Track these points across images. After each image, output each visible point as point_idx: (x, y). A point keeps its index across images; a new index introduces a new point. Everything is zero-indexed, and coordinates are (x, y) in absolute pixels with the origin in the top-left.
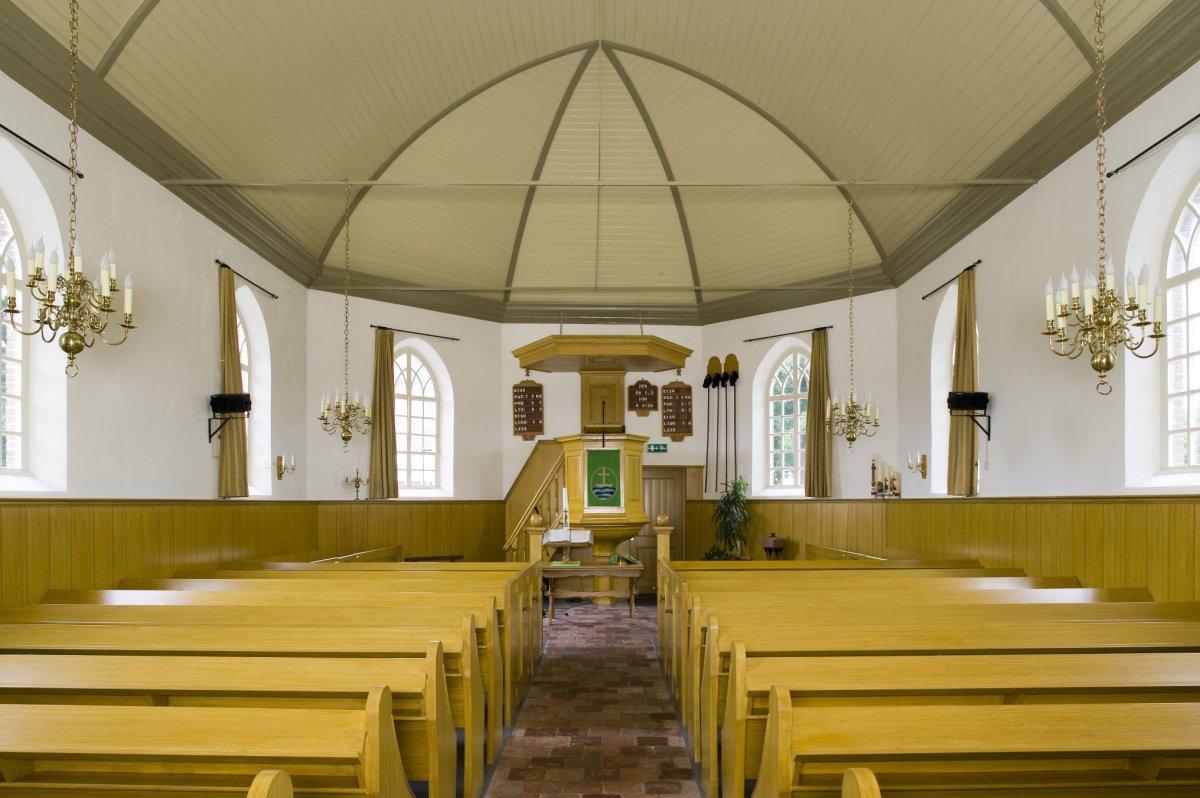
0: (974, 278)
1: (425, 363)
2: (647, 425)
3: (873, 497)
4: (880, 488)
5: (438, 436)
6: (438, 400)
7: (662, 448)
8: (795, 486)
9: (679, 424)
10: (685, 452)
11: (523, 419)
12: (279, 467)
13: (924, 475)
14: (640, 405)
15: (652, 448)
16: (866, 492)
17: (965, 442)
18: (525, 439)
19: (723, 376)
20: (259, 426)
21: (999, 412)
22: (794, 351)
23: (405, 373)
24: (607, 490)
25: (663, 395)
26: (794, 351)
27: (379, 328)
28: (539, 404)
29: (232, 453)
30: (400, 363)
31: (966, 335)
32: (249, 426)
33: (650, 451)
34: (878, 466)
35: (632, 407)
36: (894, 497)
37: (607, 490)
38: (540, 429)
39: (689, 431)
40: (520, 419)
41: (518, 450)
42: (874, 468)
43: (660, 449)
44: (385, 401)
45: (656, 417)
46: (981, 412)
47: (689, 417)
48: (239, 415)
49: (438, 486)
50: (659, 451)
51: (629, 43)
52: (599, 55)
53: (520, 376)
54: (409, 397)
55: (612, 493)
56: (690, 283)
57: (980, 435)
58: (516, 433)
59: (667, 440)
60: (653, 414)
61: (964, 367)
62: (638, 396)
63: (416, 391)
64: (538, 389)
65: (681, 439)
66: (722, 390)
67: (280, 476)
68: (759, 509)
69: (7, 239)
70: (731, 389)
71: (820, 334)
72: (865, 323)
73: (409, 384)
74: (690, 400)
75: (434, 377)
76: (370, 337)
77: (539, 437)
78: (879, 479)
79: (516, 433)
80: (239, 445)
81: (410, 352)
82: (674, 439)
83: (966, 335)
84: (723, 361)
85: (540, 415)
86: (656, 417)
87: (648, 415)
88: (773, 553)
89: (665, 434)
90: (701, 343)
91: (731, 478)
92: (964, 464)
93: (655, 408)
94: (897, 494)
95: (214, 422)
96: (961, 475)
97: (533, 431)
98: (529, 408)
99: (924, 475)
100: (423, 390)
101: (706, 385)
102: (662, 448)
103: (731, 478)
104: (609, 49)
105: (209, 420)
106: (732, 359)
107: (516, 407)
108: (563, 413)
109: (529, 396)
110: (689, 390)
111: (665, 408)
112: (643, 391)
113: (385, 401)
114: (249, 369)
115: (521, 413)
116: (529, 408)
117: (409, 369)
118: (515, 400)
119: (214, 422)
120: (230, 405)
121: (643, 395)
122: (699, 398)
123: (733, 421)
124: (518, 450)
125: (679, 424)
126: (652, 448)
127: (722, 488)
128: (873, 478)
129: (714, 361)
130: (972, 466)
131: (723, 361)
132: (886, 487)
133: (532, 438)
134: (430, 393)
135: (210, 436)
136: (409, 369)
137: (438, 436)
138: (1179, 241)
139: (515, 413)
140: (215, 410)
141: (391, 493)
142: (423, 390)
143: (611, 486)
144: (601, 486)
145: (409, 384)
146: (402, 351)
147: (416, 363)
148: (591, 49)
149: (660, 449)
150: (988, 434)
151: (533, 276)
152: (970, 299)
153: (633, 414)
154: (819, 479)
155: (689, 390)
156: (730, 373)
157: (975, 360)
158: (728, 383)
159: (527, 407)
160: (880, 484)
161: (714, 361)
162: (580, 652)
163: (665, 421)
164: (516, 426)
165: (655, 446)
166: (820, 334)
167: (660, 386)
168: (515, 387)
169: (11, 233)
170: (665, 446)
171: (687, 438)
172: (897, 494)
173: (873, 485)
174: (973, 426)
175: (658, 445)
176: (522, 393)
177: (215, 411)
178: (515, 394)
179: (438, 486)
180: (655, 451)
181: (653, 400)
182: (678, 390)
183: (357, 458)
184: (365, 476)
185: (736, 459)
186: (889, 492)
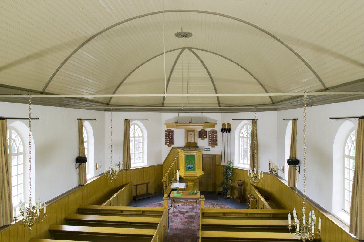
0: (296, 123)
1: (139, 127)
2: (203, 143)
3: (269, 172)
4: (272, 170)
5: (143, 147)
6: (143, 137)
7: (208, 149)
8: (247, 164)
9: (214, 142)
10: (216, 151)
11: (168, 141)
12: (97, 167)
13: (283, 172)
14: (202, 136)
15: (206, 149)
16: (267, 171)
17: (293, 172)
18: (169, 146)
19: (226, 129)
20: (90, 166)
21: (302, 165)
22: (247, 124)
23: (133, 130)
24: (191, 167)
25: (209, 134)
26: (247, 124)
27: (126, 119)
28: (172, 136)
29: (82, 172)
30: (132, 128)
31: (293, 141)
32: (88, 167)
33: (205, 150)
34: (271, 163)
35: (200, 137)
36: (275, 174)
37: (191, 167)
38: (173, 144)
39: (216, 144)
40: (167, 141)
41: (166, 150)
42: (270, 164)
43: (208, 150)
44: (127, 145)
45: (207, 140)
46: (298, 166)
47: (216, 140)
48: (84, 163)
49: (143, 162)
50: (208, 150)
51: (195, 47)
52: (186, 50)
53: (167, 129)
54: (134, 137)
55: (193, 167)
56: (217, 102)
57: (297, 172)
58: (166, 145)
59: (210, 147)
60: (206, 139)
61: (293, 148)
62: (201, 134)
63: (137, 135)
64: (172, 132)
65: (214, 147)
66: (226, 134)
67: (97, 169)
68: (237, 171)
69: (20, 141)
70: (229, 134)
71: (254, 121)
72: (267, 120)
73: (134, 133)
74: (217, 135)
75: (142, 130)
76: (123, 123)
77: (172, 146)
78: (271, 167)
79: (166, 145)
80: (84, 169)
81: (134, 124)
82: (212, 147)
83: (293, 141)
84: (226, 125)
85: (172, 139)
86: (207, 140)
87: (204, 139)
88: (240, 186)
89: (209, 145)
90: (219, 119)
91: (229, 160)
92: (292, 179)
93: (207, 137)
94: (276, 173)
95: (77, 165)
96: (292, 182)
97: (170, 144)
98: (170, 138)
99: (283, 172)
100: (139, 135)
101: (221, 131)
102: (208, 149)
103: (229, 160)
104: (190, 49)
105: (76, 165)
106: (229, 124)
107: (166, 137)
108: (180, 140)
109: (170, 134)
110: (216, 132)
111: (210, 137)
112: (203, 132)
113: (127, 145)
114: (87, 141)
115: (167, 139)
116: (170, 138)
117: (134, 129)
118: (166, 135)
119: (77, 165)
120: (81, 160)
121: (203, 134)
122: (220, 135)
123: (229, 143)
124: (166, 150)
125: (214, 142)
126: (206, 149)
127: (226, 162)
128: (270, 167)
129: (224, 124)
130: (295, 180)
131: (226, 125)
132: (273, 170)
133: (171, 146)
134: (141, 135)
135: (76, 169)
136: (134, 129)
137: (143, 147)
138: (351, 137)
139: (166, 139)
140: (77, 162)
141: (129, 167)
142: (139, 135)
143: (192, 165)
144: (190, 165)
145: (134, 133)
146: (132, 125)
147: (136, 127)
148: (184, 49)
149: (208, 150)
150: (299, 172)
151: (171, 97)
152: (295, 129)
153: (200, 139)
154: (254, 163)
155: (216, 132)
156: (229, 128)
157: (296, 148)
158: (228, 131)
159: (169, 137)
160: (271, 169)
161: (224, 124)
162: (178, 232)
163: (209, 141)
164: (166, 143)
165: (206, 149)
166: (254, 121)
167: (208, 131)
168: (165, 131)
169: (20, 140)
170: (209, 149)
171: (216, 146)
172: (276, 173)
173: (270, 169)
174: (295, 170)
175: (207, 149)
176: (168, 133)
177: (77, 162)
178: (165, 133)
179: (143, 162)
180: (206, 150)
181: (206, 135)
182: (213, 132)
183: (119, 158)
184: (121, 163)
185: (230, 155)
186: (274, 172)
